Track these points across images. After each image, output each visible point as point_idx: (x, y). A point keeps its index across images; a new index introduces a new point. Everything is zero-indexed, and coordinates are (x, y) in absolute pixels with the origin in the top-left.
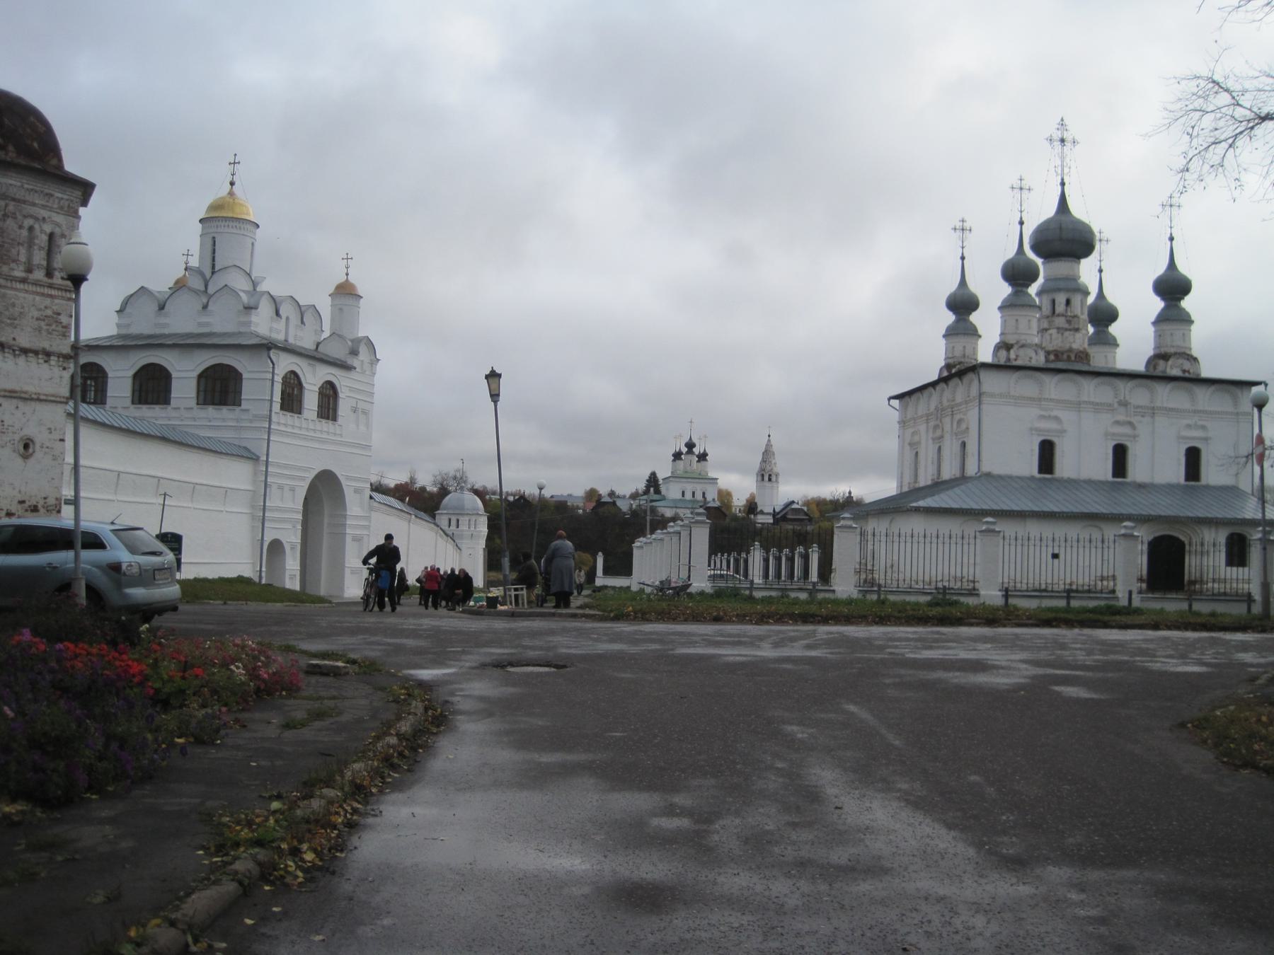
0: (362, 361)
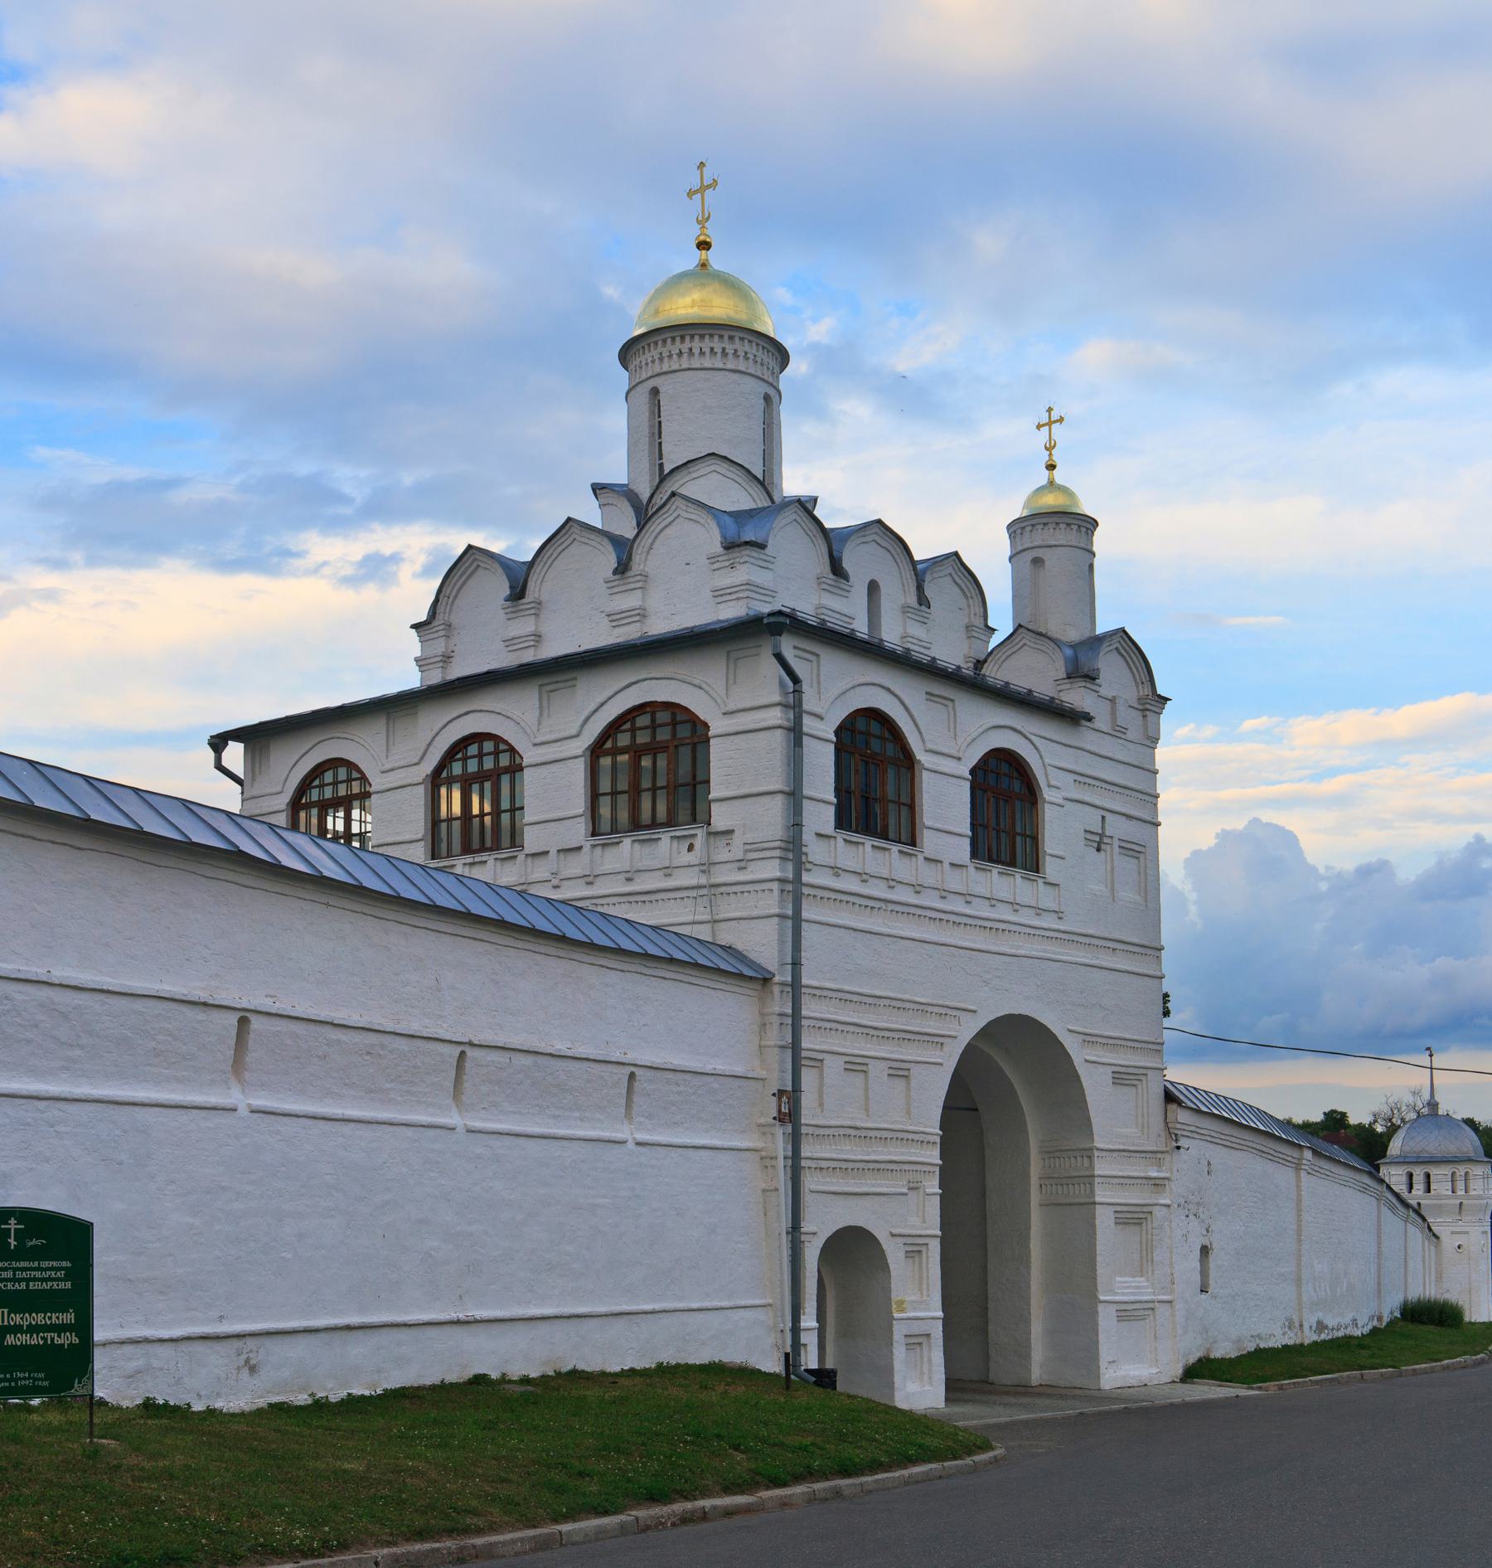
0: (1113, 701)
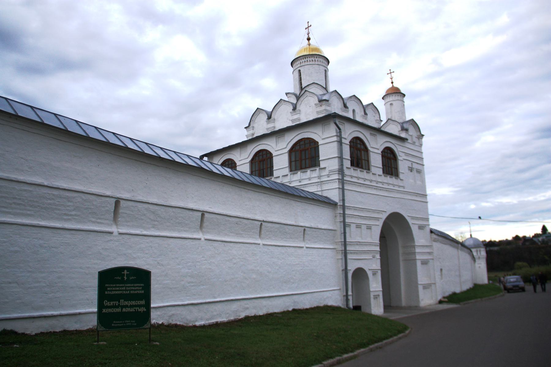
0: (411, 136)
